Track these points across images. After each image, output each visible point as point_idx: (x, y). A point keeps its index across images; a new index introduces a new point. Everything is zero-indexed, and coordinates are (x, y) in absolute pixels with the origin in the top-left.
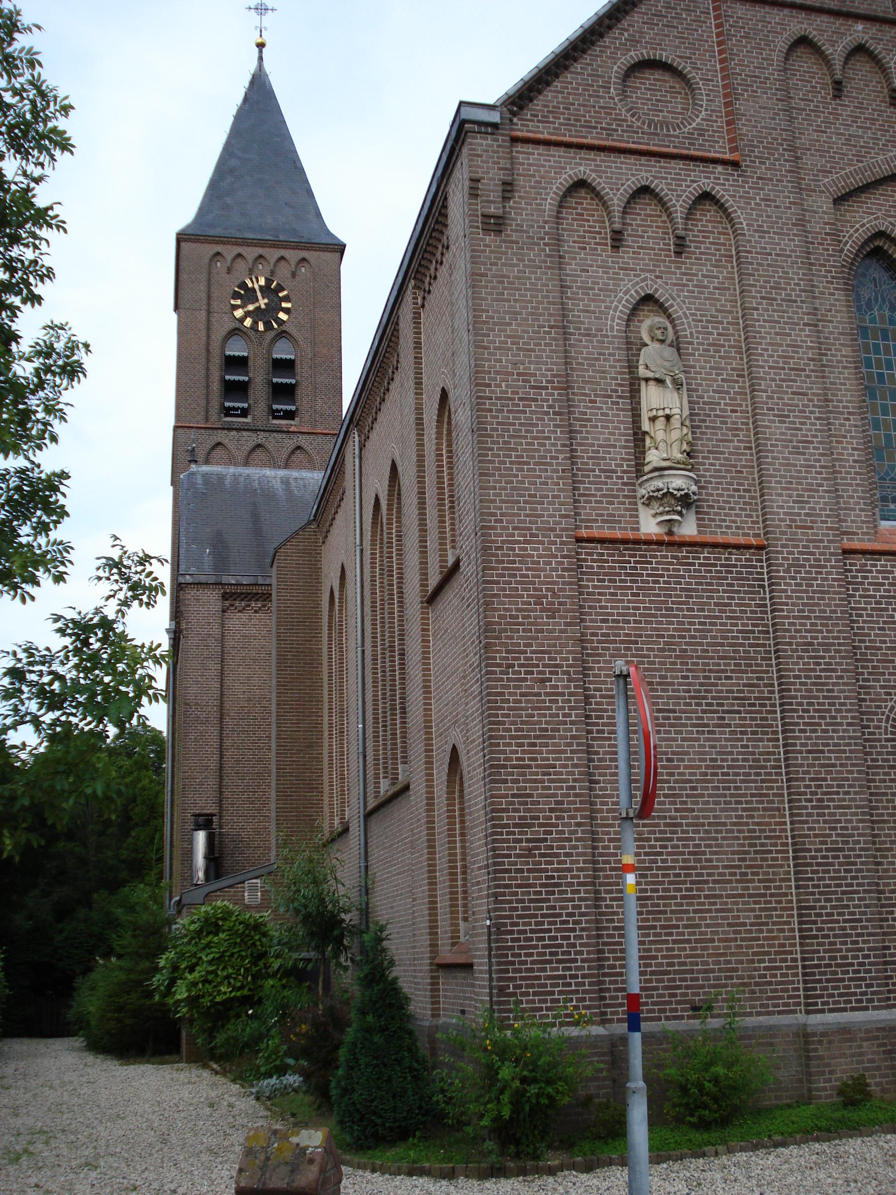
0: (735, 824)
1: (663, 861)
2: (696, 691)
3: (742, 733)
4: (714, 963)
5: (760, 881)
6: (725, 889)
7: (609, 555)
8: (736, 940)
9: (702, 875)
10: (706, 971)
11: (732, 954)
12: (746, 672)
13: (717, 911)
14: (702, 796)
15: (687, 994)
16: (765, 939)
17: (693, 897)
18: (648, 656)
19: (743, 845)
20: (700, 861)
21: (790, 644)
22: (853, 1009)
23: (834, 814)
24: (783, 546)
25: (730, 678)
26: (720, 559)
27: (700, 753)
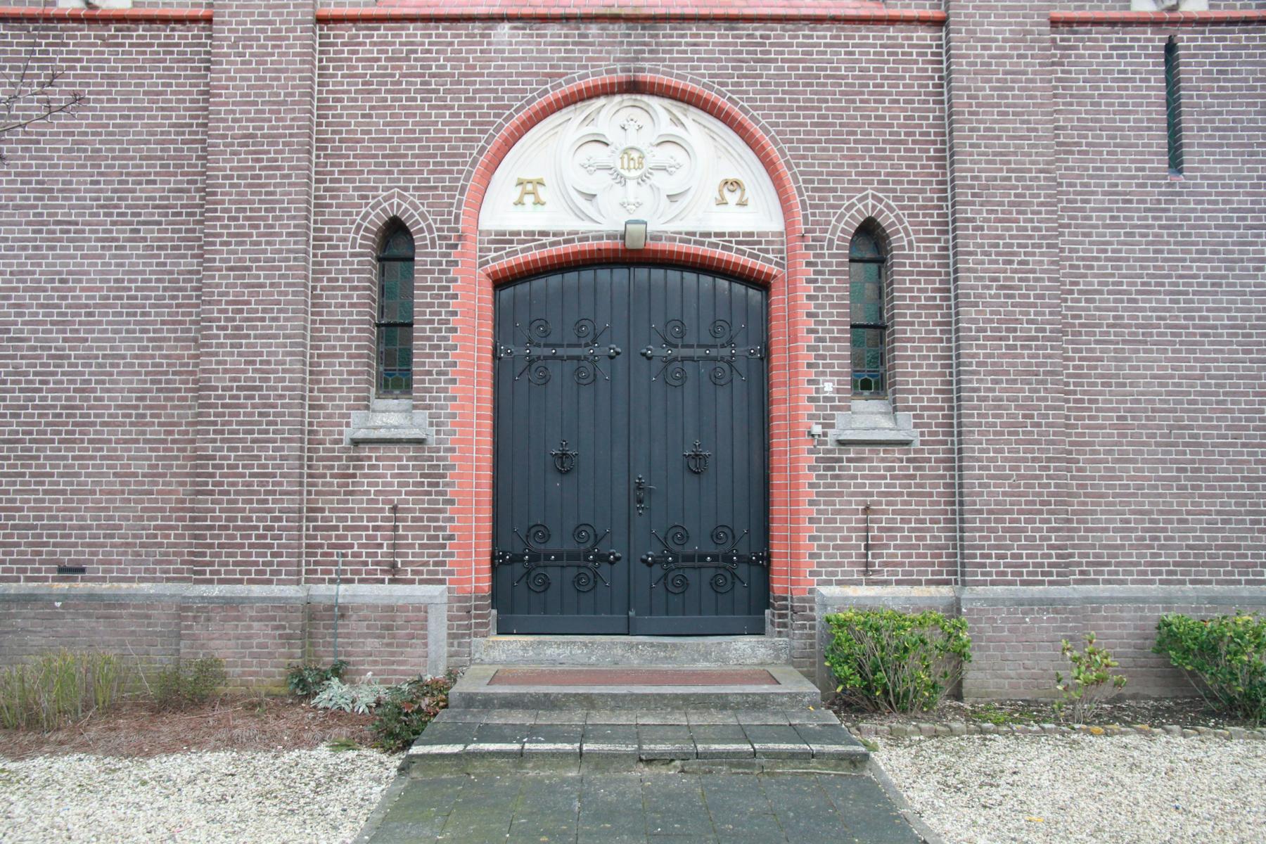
0: (137, 357)
1: (41, 399)
2: (106, 199)
3: (159, 248)
4: (93, 518)
5: (160, 424)
6: (115, 433)
7: (13, 36)
8: (123, 492)
9: (88, 416)
10: (81, 528)
11: (116, 509)
12: (175, 174)
13: (103, 458)
14: (100, 323)
15: (54, 553)
16: (159, 492)
17: (74, 441)
18: (51, 158)
19: (145, 382)
20: (87, 399)
21: (224, 137)
22: (251, 581)
23: (254, 345)
24: (232, 15)
25: (154, 182)
26: (158, 37)
27: (102, 273)
